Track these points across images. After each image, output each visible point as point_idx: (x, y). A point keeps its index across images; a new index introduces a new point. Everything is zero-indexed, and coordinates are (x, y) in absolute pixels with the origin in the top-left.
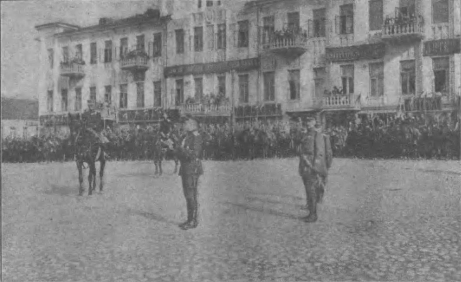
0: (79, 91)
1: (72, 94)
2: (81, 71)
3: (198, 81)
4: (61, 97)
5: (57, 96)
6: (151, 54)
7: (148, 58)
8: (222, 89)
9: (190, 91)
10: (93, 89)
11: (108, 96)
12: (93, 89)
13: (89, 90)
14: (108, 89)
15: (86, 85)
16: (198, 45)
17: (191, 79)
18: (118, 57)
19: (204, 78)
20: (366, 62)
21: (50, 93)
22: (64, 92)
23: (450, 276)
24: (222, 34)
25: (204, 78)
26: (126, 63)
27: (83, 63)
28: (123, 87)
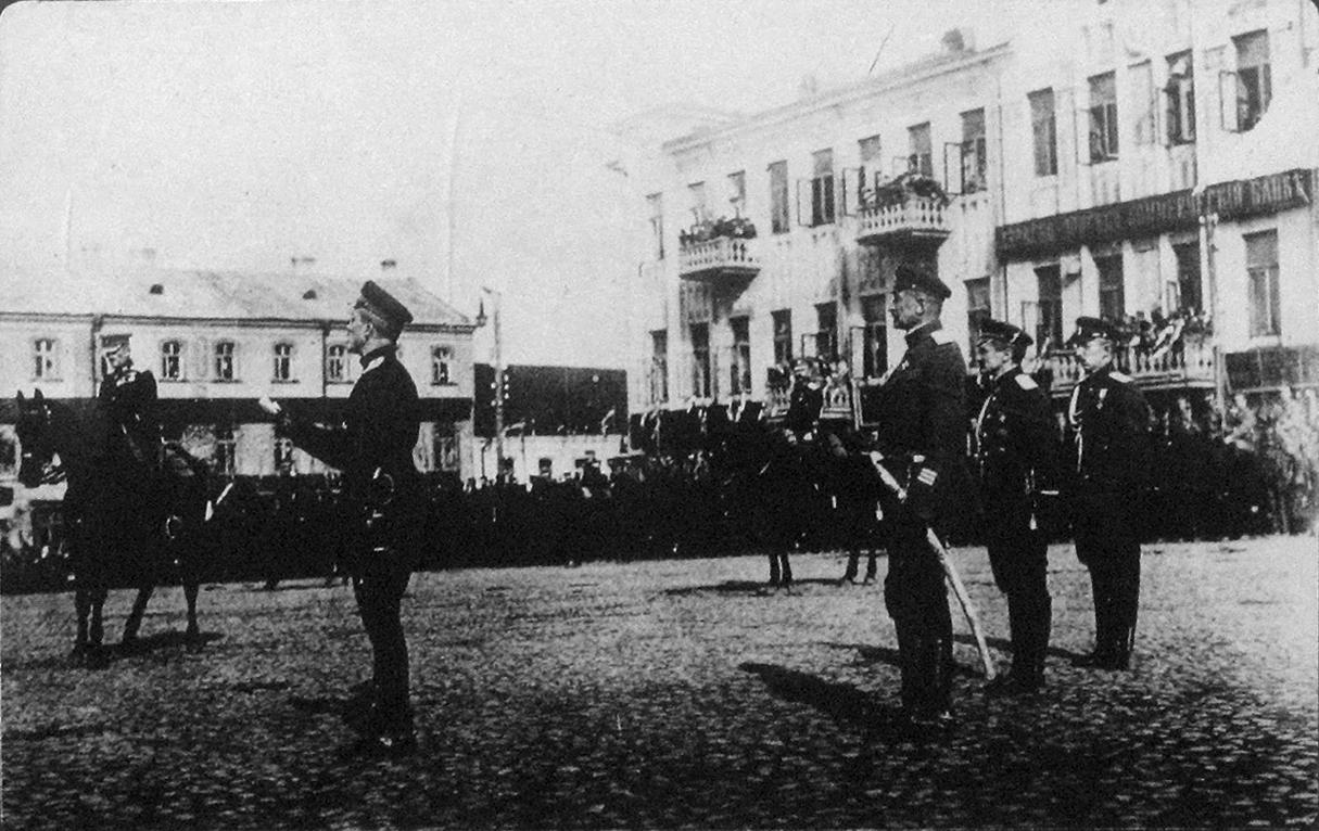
0: (740, 326)
1: (721, 337)
2: (353, 320)
3: (1111, 270)
4: (690, 349)
5: (680, 350)
6: (954, 187)
7: (945, 201)
8: (1190, 290)
9: (1082, 302)
10: (782, 318)
11: (826, 338)
12: (782, 318)
13: (770, 321)
14: (827, 314)
15: (757, 302)
16: (1103, 147)
17: (1082, 262)
18: (853, 204)
19: (1128, 253)
20: (1168, 234)
21: (660, 337)
22: (699, 335)
23: (388, 829)
24: (1184, 87)
25: (1128, 253)
26: (873, 220)
27: (750, 233)
28: (699, 335)
